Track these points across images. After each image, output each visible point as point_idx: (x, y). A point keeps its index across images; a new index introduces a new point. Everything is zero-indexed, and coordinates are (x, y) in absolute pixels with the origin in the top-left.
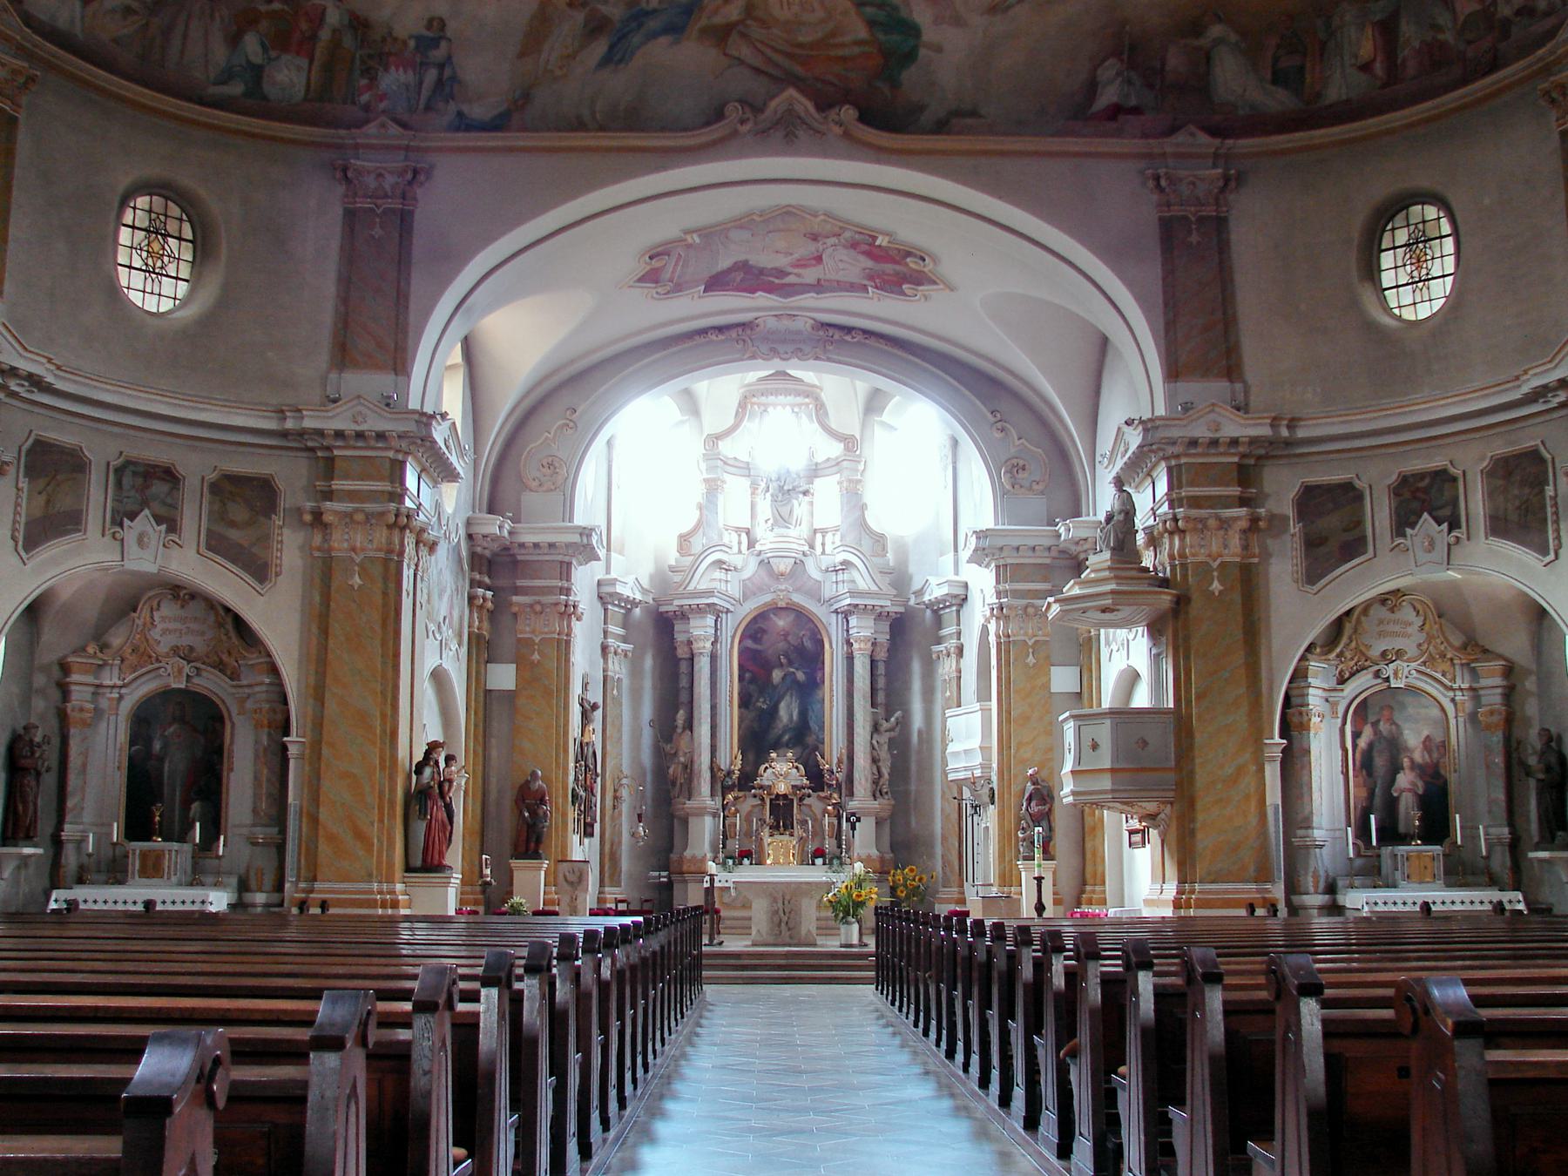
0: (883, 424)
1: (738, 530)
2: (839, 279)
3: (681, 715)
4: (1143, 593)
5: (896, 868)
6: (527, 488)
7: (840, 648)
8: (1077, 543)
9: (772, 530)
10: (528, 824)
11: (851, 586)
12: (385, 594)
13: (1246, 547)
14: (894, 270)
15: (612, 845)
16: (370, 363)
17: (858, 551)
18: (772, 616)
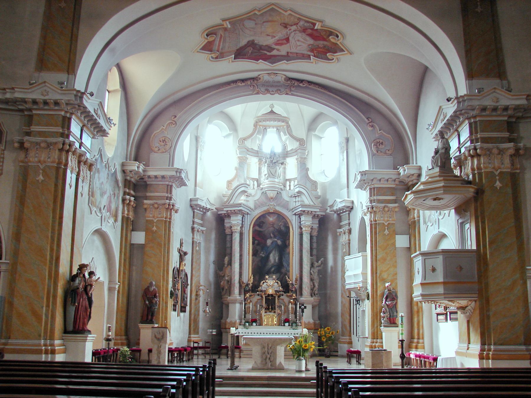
0: (316, 135)
1: (253, 179)
2: (298, 52)
3: (227, 259)
4: (458, 187)
5: (321, 328)
6: (152, 151)
7: (297, 230)
8: (408, 177)
9: (267, 179)
10: (148, 308)
11: (302, 203)
12: (56, 185)
13: (513, 165)
14: (323, 44)
15: (195, 316)
16: (56, 68)
17: (305, 187)
18: (267, 216)
